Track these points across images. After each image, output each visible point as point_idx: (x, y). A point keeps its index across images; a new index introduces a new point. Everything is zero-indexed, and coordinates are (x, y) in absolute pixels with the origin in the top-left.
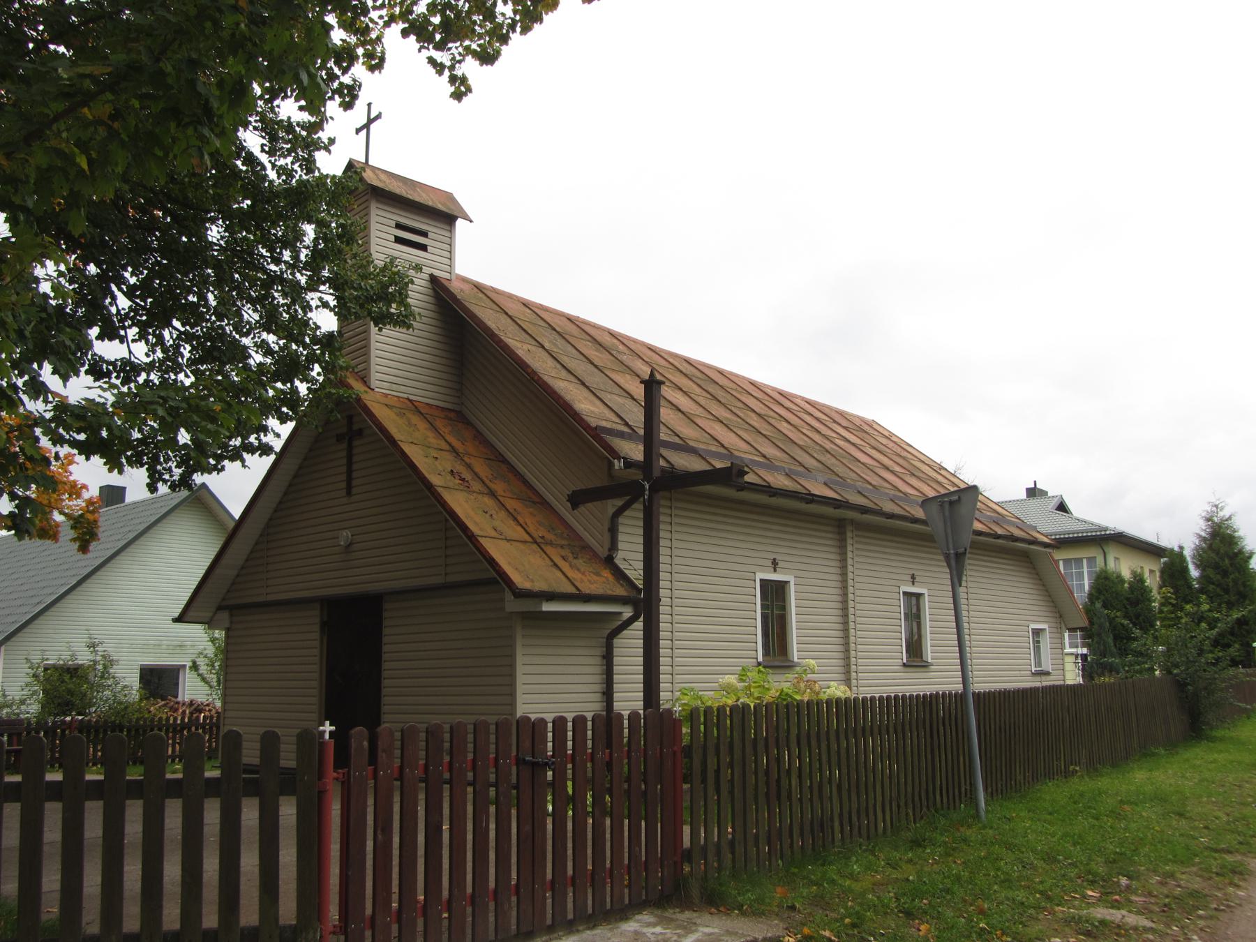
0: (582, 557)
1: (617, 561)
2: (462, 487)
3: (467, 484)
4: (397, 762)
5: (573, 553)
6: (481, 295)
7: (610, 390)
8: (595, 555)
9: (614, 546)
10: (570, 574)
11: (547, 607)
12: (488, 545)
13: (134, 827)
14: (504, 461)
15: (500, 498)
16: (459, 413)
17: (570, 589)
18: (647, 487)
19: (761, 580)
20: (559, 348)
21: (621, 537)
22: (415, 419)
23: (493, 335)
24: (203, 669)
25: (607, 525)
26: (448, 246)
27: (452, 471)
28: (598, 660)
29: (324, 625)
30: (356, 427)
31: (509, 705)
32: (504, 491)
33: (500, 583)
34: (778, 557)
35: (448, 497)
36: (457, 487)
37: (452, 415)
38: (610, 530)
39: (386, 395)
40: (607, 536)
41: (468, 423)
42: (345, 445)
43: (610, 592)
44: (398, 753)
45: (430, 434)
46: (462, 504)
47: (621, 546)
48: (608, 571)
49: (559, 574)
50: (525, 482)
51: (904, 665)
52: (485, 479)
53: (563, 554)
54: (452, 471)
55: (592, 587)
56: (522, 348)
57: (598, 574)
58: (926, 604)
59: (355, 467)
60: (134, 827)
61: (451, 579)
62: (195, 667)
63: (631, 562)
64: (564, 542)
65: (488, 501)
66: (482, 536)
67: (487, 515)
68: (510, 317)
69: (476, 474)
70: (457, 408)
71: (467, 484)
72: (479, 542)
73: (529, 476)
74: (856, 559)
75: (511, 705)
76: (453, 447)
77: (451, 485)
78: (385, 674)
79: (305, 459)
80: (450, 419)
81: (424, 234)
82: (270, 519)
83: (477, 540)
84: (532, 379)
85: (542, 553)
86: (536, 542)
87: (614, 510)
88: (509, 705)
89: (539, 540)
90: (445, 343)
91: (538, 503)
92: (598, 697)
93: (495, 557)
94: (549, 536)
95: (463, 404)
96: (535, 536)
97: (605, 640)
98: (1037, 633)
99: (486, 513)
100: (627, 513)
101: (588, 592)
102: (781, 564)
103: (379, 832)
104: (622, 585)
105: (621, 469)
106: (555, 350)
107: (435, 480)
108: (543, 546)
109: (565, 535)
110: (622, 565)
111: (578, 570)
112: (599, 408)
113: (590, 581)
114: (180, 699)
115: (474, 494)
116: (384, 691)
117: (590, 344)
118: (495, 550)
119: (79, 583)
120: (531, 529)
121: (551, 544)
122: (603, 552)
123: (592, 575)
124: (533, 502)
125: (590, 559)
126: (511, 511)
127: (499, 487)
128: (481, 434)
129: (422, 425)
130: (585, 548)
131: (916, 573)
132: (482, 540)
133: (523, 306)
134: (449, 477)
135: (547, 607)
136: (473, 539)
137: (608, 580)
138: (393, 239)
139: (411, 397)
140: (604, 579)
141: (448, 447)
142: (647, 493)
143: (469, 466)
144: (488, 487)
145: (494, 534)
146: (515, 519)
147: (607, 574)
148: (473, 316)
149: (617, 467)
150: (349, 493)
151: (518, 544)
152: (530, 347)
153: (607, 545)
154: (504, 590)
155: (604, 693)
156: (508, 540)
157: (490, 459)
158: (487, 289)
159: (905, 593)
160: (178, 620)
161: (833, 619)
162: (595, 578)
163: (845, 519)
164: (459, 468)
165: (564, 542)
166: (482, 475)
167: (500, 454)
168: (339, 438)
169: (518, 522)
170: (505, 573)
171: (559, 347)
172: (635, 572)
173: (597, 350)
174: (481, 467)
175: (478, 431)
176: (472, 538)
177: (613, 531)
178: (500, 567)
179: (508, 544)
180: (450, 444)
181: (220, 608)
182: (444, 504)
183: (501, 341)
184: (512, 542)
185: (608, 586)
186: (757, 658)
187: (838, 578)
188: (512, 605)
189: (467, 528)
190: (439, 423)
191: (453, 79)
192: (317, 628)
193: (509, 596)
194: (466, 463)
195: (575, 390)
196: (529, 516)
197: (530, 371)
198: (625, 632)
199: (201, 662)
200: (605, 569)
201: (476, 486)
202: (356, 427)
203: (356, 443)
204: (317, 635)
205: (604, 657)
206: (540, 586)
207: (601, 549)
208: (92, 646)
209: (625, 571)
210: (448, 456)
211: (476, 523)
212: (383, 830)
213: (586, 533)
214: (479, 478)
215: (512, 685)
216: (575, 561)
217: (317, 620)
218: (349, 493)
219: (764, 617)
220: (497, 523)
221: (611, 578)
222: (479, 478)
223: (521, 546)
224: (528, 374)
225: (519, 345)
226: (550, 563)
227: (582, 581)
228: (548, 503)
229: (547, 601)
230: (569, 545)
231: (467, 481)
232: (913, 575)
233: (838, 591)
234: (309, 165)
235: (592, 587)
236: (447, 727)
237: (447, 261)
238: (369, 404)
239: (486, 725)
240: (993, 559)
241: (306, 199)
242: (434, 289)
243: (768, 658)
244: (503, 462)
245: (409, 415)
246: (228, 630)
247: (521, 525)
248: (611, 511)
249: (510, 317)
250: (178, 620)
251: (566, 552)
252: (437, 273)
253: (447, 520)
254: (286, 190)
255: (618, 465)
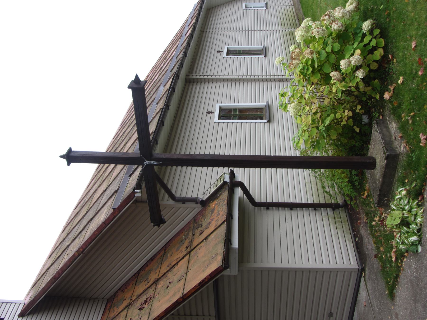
0: (201, 221)
1: (204, 199)
2: (150, 303)
3: (149, 300)
5: (198, 228)
7: (98, 204)
8: (200, 213)
9: (195, 200)
10: (212, 229)
11: (236, 244)
12: (188, 289)
14: (138, 273)
15: (160, 276)
17: (223, 228)
18: (147, 162)
19: (219, 119)
20: (72, 236)
21: (189, 196)
25: (180, 205)
26: (8, 304)
27: (139, 309)
28: (270, 212)
31: (309, 273)
32: (156, 273)
33: (217, 279)
34: (206, 111)
36: (150, 306)
37: (109, 305)
38: (184, 203)
40: (188, 205)
41: (115, 295)
43: (226, 202)
47: (195, 196)
48: (211, 205)
49: (212, 236)
50: (152, 259)
51: (265, 56)
52: (147, 286)
53: (198, 234)
54: (139, 309)
55: (221, 213)
56: (66, 258)
57: (213, 211)
58: (233, 47)
61: (213, 312)
63: (205, 190)
64: (191, 234)
65: (161, 284)
66: (183, 291)
67: (170, 286)
69: (143, 292)
70: (105, 302)
71: (149, 300)
72: (187, 293)
73: (148, 257)
74: (208, 74)
75: (303, 271)
76: (126, 307)
77: (148, 311)
80: (111, 307)
83: (186, 294)
84: (82, 252)
85: (197, 248)
86: (190, 252)
87: (171, 200)
88: (309, 273)
89: (188, 250)
90: (89, 302)
91: (165, 251)
92: (294, 213)
93: (198, 282)
94: (186, 244)
95: (103, 298)
96: (185, 253)
97: (256, 208)
98: (246, 7)
99: (168, 286)
100: (173, 192)
101: (225, 216)
102: (210, 110)
104: (220, 195)
105: (141, 192)
106: (72, 238)
108: (192, 248)
109: (186, 233)
110: (208, 195)
111: (209, 223)
112: (105, 209)
113: (218, 215)
115: (156, 294)
117: (76, 219)
120: (181, 255)
121: (191, 242)
122: (198, 208)
123: (213, 214)
124: (164, 254)
125: (203, 216)
126: (168, 268)
127: (153, 277)
128: (121, 287)
130: (195, 219)
131: (217, 50)
132: (187, 290)
133: (50, 258)
134: (143, 312)
135: (236, 244)
136: (185, 297)
137: (217, 204)
140: (216, 206)
142: (152, 162)
143: (138, 297)
144: (152, 284)
145: (182, 282)
146: (174, 266)
147: (213, 205)
149: (140, 195)
151: (190, 265)
152: (66, 254)
153: (193, 205)
154: (223, 275)
155: (291, 209)
156: (187, 271)
157: (136, 282)
158: (37, 279)
159: (227, 55)
161: (241, 86)
162: (216, 211)
163: (186, 79)
164: (138, 304)
165: (191, 234)
166: (145, 287)
167: (134, 275)
169: (175, 264)
170: (210, 275)
171: (71, 236)
172: (212, 187)
173: (79, 215)
175: (120, 289)
176: (184, 298)
177: (184, 200)
178: (205, 278)
179: (190, 271)
180: (124, 309)
184: (189, 269)
185: (221, 203)
186: (265, 123)
187: (218, 84)
188: (233, 270)
189: (177, 302)
193: (226, 272)
194: (136, 299)
195: (93, 225)
196: (172, 259)
197: (77, 254)
198: (251, 192)
200: (209, 206)
201: (151, 292)
205: (268, 209)
206: (220, 249)
207: (196, 209)
209: (211, 193)
210: (130, 311)
211: (174, 295)
213: (185, 220)
214: (146, 290)
215: (289, 270)
216: (204, 226)
219: (239, 119)
220: (176, 279)
221: (216, 202)
222: (146, 290)
223: (191, 262)
224: (79, 255)
226: (204, 242)
227: (217, 220)
228: (166, 244)
229: (231, 244)
230: (192, 230)
231: (147, 299)
232: (217, 51)
233: (226, 84)
235: (221, 213)
237: (13, 305)
240: (209, 27)
242: (28, 315)
243: (264, 118)
244: (139, 274)
247: (178, 262)
248: (171, 202)
251: (197, 232)
252: (19, 312)
253: (172, 314)
255: (138, 194)
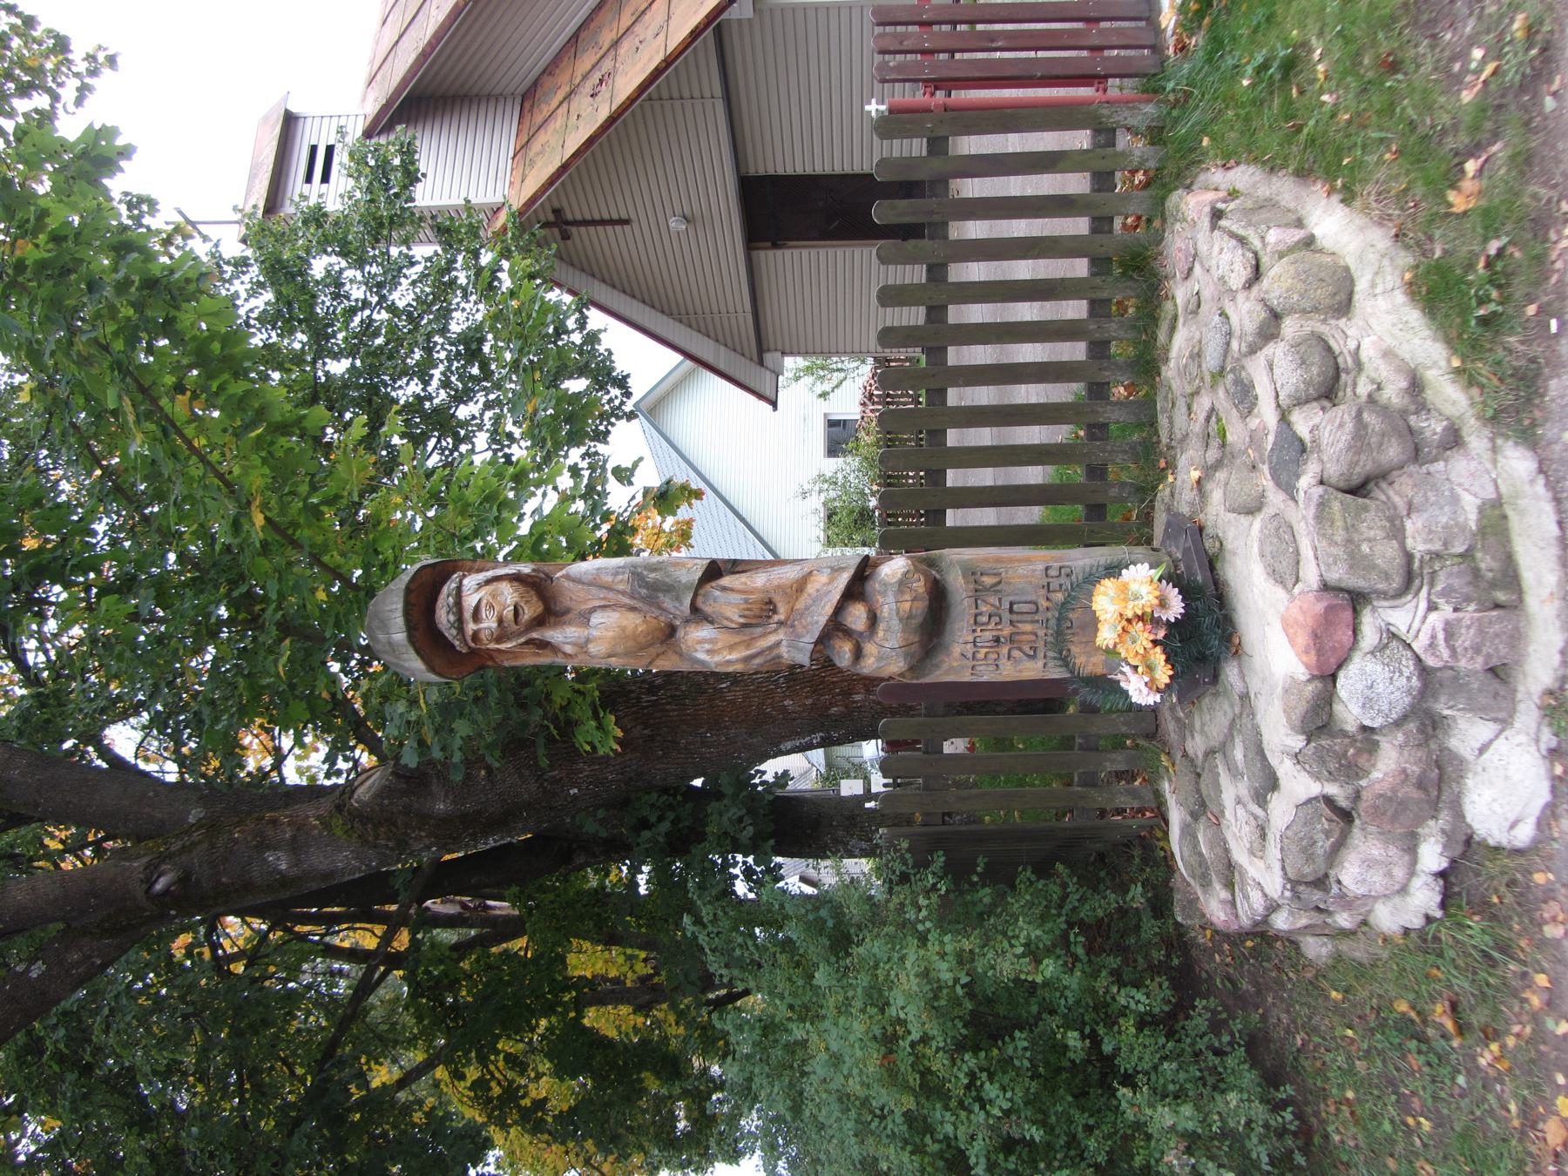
4: (916, 28)
6: (379, 77)
12: (673, 44)
13: (977, 313)
14: (575, 38)
16: (524, 98)
22: (536, 146)
23: (424, 55)
24: (827, 387)
29: (775, 246)
30: (552, 218)
35: (621, 97)
37: (527, 105)
39: (511, 183)
41: (535, 84)
42: (574, 230)
44: (900, 29)
45: (551, 126)
46: (627, 81)
59: (597, 217)
60: (977, 313)
61: (718, 91)
62: (824, 395)
65: (625, 46)
68: (401, 37)
69: (594, 67)
70: (518, 101)
77: (608, 95)
78: (828, 171)
79: (593, 276)
81: (314, 149)
82: (663, 312)
103: (994, 45)
107: (603, 114)
114: (858, 417)
116: (848, 170)
118: (680, 32)
119: (743, 520)
127: (607, 38)
129: (542, 138)
134: (598, 98)
138: (313, 142)
139: (511, 154)
141: (565, 105)
143: (585, 77)
145: (662, 37)
146: (644, 12)
148: (405, 81)
150: (627, 222)
160: (774, 404)
164: (588, 87)
166: (594, 59)
168: (566, 236)
174: (586, 61)
176: (668, 62)
181: (761, 363)
182: (631, 100)
183: (430, 43)
190: (538, 119)
191: (93, 73)
192: (779, 252)
199: (819, 389)
201: (607, 65)
202: (552, 218)
203: (570, 217)
204: (788, 252)
208: (804, 495)
211: (650, 60)
212: (992, 41)
217: (771, 253)
218: (627, 222)
225: (432, 21)
234: (241, 264)
236: (878, 58)
238: (523, 201)
239: (882, 67)
241: (279, 261)
245: (531, 154)
246: (784, 353)
249: (401, 37)
250: (774, 404)
254: (272, 284)
